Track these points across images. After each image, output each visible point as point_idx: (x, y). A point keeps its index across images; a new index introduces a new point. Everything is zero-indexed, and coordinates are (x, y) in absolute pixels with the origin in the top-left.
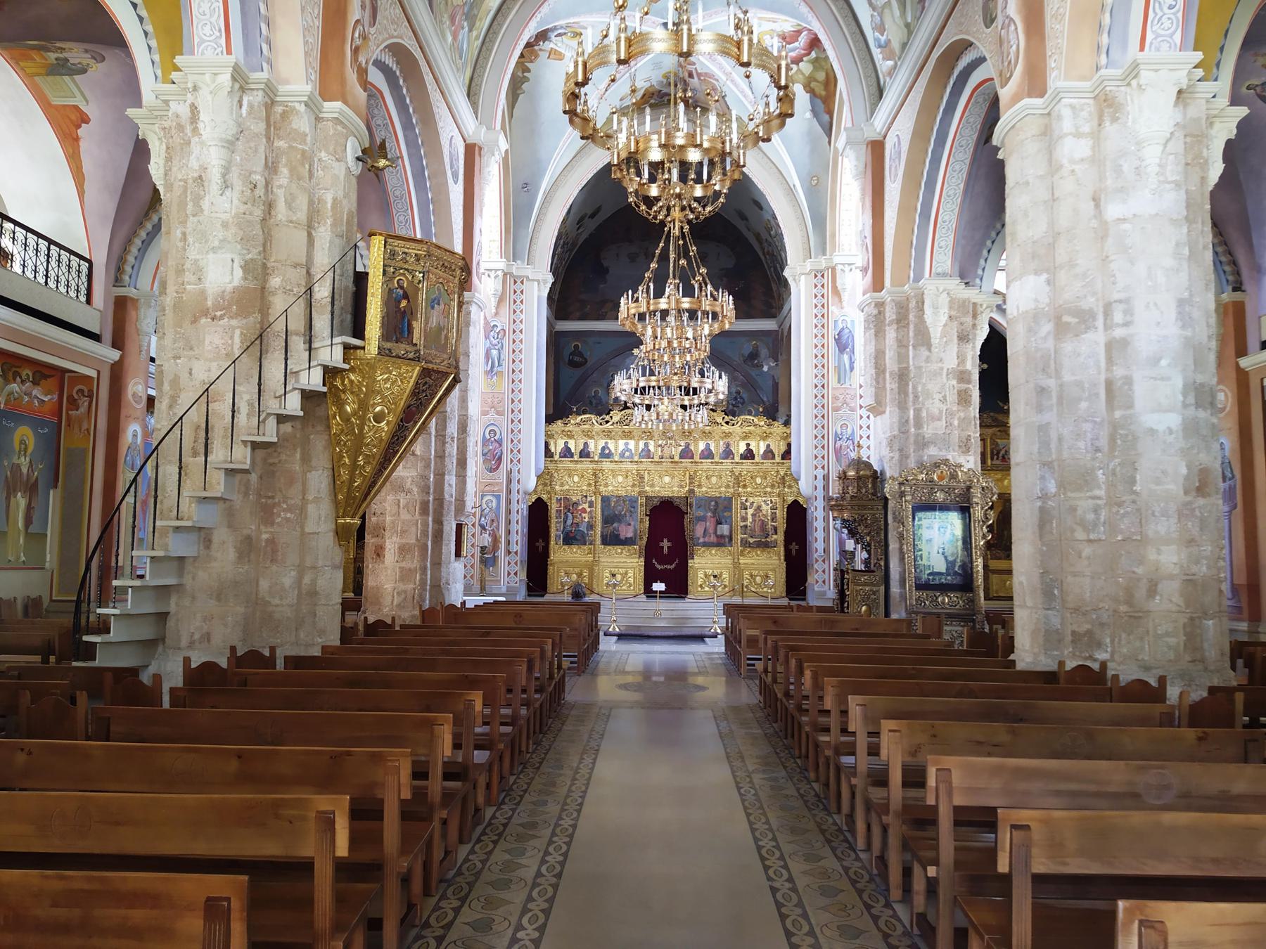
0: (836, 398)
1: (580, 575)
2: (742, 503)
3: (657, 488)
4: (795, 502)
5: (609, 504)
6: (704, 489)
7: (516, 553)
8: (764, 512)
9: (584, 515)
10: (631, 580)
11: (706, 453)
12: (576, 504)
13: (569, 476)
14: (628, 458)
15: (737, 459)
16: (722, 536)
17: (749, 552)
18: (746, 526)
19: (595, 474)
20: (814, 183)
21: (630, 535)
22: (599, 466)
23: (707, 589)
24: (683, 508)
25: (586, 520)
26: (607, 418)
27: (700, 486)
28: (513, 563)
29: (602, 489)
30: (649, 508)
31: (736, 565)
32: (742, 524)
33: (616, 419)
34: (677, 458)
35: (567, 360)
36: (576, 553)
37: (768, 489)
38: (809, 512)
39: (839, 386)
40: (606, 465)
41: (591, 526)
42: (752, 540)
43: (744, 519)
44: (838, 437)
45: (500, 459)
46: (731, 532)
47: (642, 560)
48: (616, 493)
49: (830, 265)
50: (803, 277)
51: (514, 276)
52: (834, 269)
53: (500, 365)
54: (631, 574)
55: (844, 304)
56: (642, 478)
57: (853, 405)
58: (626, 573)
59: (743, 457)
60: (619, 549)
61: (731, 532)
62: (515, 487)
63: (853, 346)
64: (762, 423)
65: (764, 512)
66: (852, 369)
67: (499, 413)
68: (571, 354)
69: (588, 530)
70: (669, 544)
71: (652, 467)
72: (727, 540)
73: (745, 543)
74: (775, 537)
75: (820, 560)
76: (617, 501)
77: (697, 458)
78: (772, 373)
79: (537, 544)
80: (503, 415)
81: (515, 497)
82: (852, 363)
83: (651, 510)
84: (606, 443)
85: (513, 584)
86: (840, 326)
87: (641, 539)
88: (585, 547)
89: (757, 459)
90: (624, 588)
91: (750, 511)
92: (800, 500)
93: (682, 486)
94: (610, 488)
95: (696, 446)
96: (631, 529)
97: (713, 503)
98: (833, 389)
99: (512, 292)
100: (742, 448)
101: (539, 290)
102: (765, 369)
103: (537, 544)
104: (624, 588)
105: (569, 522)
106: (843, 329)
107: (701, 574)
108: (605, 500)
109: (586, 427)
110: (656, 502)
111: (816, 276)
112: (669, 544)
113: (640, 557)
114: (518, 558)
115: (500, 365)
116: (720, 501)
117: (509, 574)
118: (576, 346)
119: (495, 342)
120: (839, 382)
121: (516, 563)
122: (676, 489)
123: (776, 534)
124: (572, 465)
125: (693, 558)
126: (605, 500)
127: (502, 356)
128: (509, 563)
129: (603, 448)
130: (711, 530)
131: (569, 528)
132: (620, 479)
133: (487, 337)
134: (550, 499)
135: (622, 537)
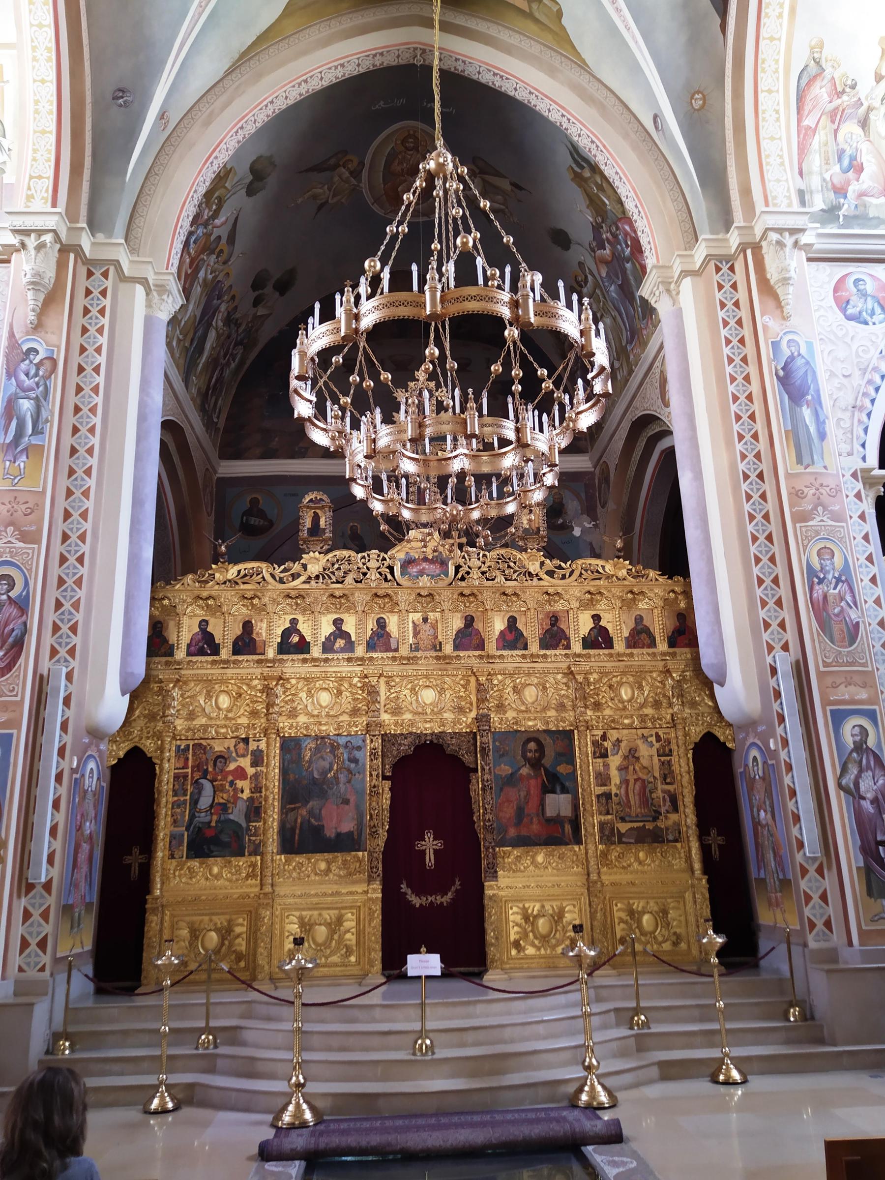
0: (797, 495)
1: (226, 933)
2: (595, 744)
3: (408, 716)
4: (709, 738)
5: (300, 757)
6: (510, 714)
7: (47, 886)
8: (644, 762)
9: (240, 784)
10: (351, 938)
11: (510, 637)
12: (223, 758)
13: (208, 696)
14: (342, 650)
15: (577, 647)
16: (557, 821)
17: (619, 857)
18: (608, 796)
19: (267, 690)
20: (697, 104)
21: (347, 826)
22: (276, 672)
23: (530, 951)
24: (467, 759)
25: (246, 795)
26: (296, 567)
27: (501, 707)
28: (36, 914)
29: (284, 723)
30: (389, 761)
31: (592, 888)
32: (600, 790)
33: (314, 569)
34: (448, 649)
35: (237, 524)
36: (217, 877)
37: (649, 711)
38: (737, 759)
39: (800, 469)
40: (293, 666)
41: (255, 811)
42: (623, 827)
43: (603, 779)
44: (814, 577)
45: (19, 645)
46: (576, 807)
47: (377, 886)
48: (314, 730)
49: (748, 239)
50: (687, 282)
51: (87, 262)
52: (757, 248)
53: (36, 431)
54: (350, 923)
55: (788, 309)
56: (373, 692)
57: (836, 508)
58: (340, 920)
59: (589, 643)
60: (321, 862)
61: (576, 807)
62: (56, 713)
63: (818, 391)
64: (623, 573)
65: (644, 762)
66: (822, 436)
67: (24, 537)
68: (244, 514)
69: (248, 819)
70: (438, 844)
71: (394, 669)
72: (568, 828)
73: (609, 835)
74: (674, 817)
75: (812, 869)
76: (318, 749)
77: (491, 647)
78: (588, 538)
79: (128, 859)
80: (38, 542)
81: (55, 738)
82: (820, 424)
83: (395, 767)
84: (294, 622)
85: (32, 974)
86: (786, 352)
87: (374, 834)
88: (241, 862)
89: (619, 646)
90: (335, 959)
91: (615, 761)
92: (721, 734)
93: (461, 710)
94: (302, 719)
95: (487, 622)
96: (350, 811)
97: (532, 745)
98: (788, 476)
99: (83, 292)
100: (584, 624)
101: (149, 305)
102: (577, 532)
103: (128, 859)
104: (335, 959)
105: (205, 802)
106: (792, 358)
107: (514, 915)
108: (291, 746)
109: (249, 588)
110: (406, 747)
111: (718, 269)
112: (438, 844)
113: (370, 880)
114: (51, 901)
115: (36, 431)
116: (547, 741)
117: (25, 944)
118: (254, 502)
119: (28, 383)
120: (799, 460)
121: (45, 915)
122: (449, 716)
123: (676, 809)
124: (216, 672)
125: (495, 876)
126: (291, 746)
127: (44, 414)
128: (27, 915)
129: (286, 634)
130: (532, 808)
131: (203, 817)
132: (325, 698)
133: (11, 373)
134: (161, 749)
135: (330, 833)
